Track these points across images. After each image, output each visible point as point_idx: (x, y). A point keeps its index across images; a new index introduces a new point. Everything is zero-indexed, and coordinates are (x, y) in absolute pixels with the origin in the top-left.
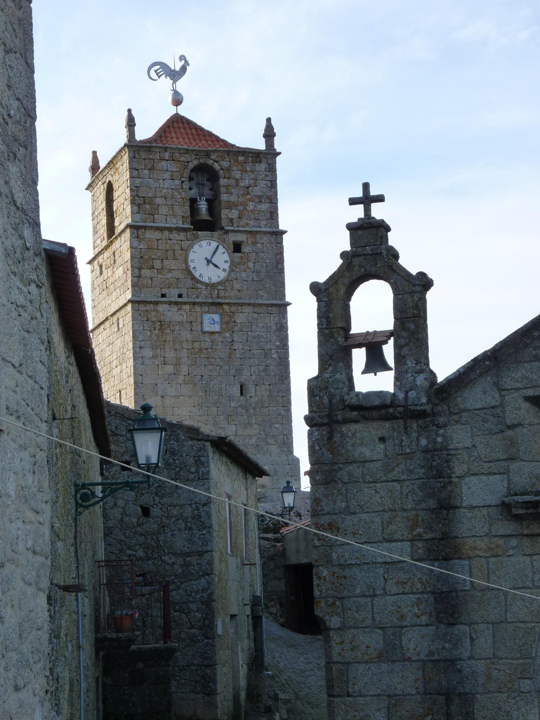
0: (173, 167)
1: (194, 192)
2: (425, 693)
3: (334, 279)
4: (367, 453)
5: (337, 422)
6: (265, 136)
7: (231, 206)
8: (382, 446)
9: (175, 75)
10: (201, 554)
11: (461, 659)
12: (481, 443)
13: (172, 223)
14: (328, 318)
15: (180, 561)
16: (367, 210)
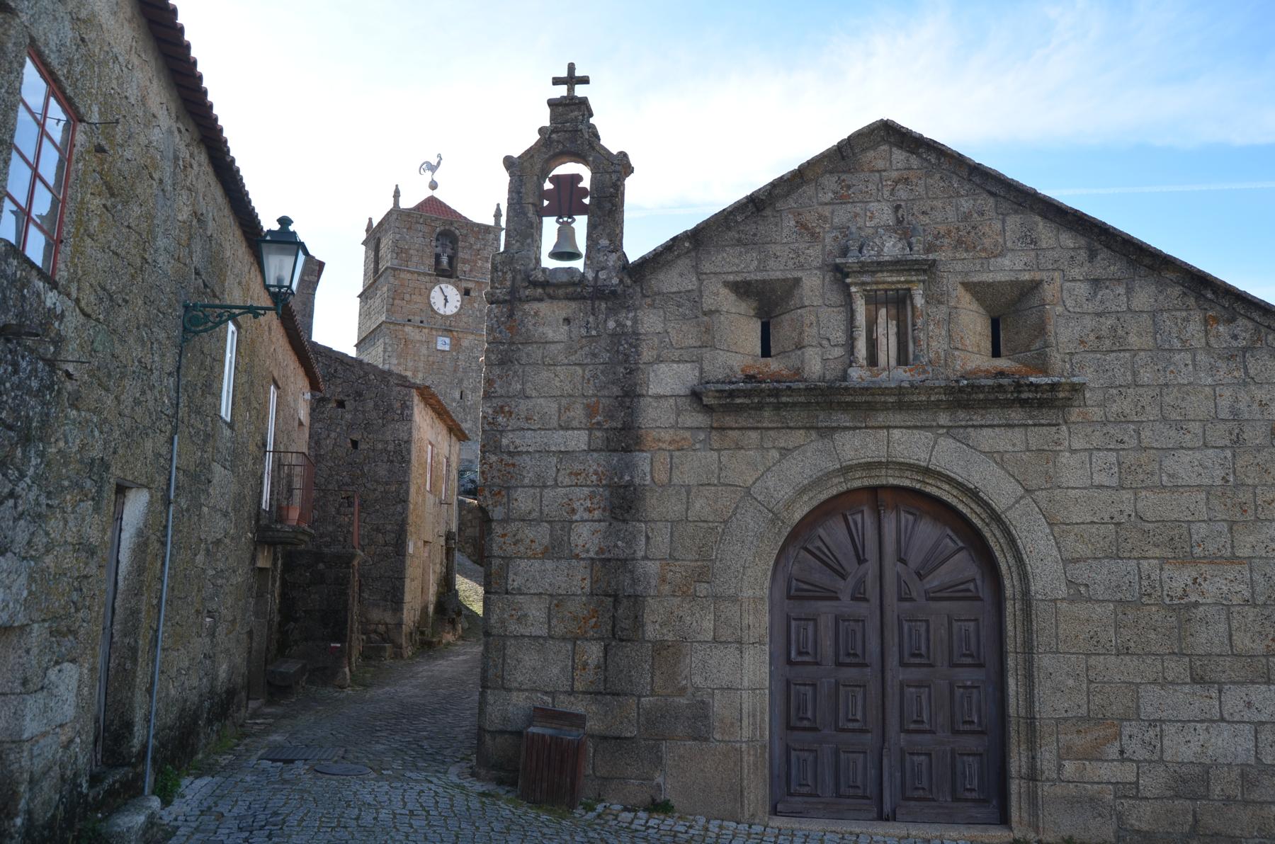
0: (426, 229)
1: (439, 250)
2: (592, 594)
3: (529, 153)
4: (550, 335)
7: (465, 262)
8: (566, 328)
9: (433, 168)
11: (633, 559)
13: (422, 269)
14: (519, 193)
15: (380, 488)
16: (571, 90)
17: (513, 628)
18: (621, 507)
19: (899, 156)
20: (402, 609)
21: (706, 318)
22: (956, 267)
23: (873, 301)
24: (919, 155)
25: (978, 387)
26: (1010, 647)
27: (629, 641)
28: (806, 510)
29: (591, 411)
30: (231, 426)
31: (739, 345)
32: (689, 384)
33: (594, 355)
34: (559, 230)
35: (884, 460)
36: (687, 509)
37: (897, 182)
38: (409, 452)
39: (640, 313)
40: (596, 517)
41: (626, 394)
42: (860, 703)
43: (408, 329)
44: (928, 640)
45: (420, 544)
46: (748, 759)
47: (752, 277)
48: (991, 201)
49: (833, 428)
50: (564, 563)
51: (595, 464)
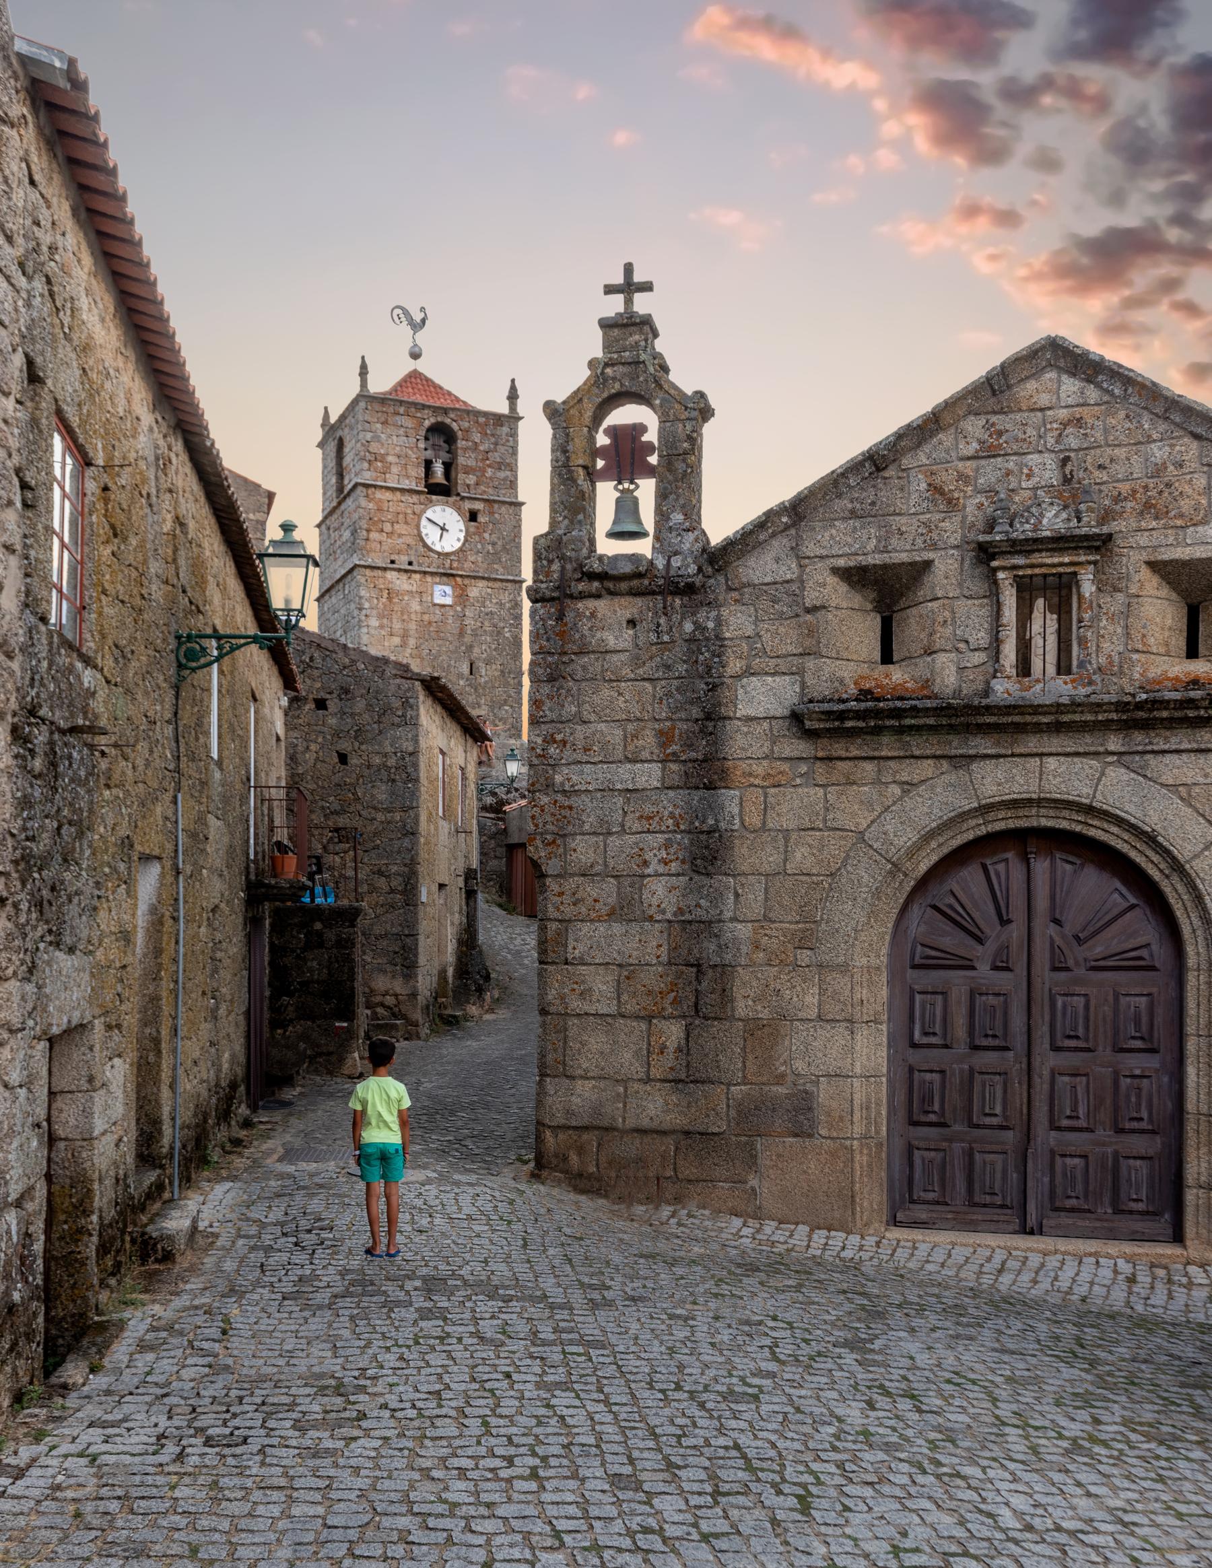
1: (429, 454)
2: (670, 963)
3: (577, 397)
4: (612, 642)
5: (571, 597)
6: (509, 398)
7: (468, 470)
8: (631, 632)
9: (418, 326)
10: (405, 809)
11: (720, 921)
12: (768, 630)
14: (565, 451)
15: (380, 817)
16: (629, 302)
17: (576, 1004)
18: (704, 858)
19: (1070, 386)
20: (416, 975)
21: (809, 617)
22: (1140, 539)
23: (1027, 590)
24: (1098, 386)
25: (1162, 702)
26: (1190, 1029)
27: (715, 1019)
28: (935, 858)
29: (664, 738)
30: (219, 763)
31: (849, 654)
32: (787, 703)
33: (668, 667)
34: (618, 501)
35: (1034, 796)
36: (785, 860)
37: (1065, 425)
38: (416, 766)
39: (725, 612)
40: (673, 871)
41: (708, 717)
42: (999, 1094)
43: (391, 575)
44: (1087, 1018)
45: (435, 888)
46: (861, 1159)
47: (871, 560)
48: (1195, 445)
49: (970, 756)
50: (635, 928)
51: (671, 804)
